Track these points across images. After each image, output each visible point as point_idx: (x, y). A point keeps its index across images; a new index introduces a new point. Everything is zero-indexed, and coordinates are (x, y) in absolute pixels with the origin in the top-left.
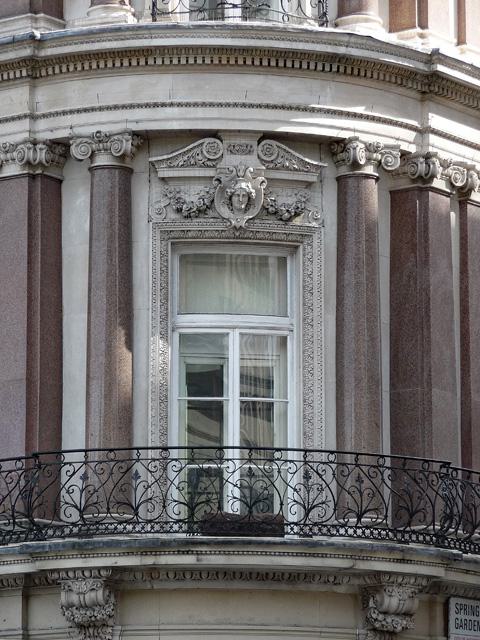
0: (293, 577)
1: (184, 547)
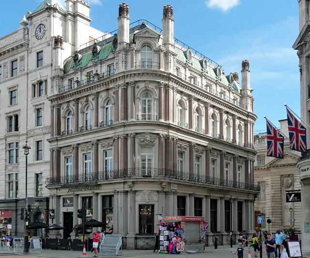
0: (153, 182)
1: (140, 179)
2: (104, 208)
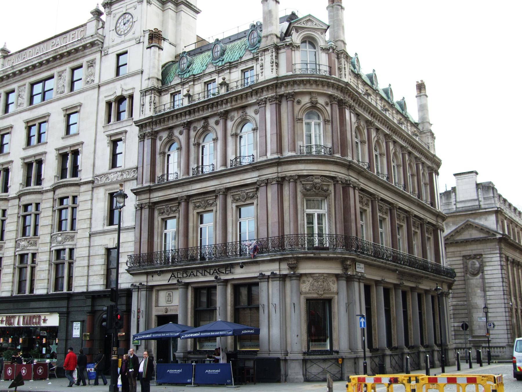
2: (237, 307)
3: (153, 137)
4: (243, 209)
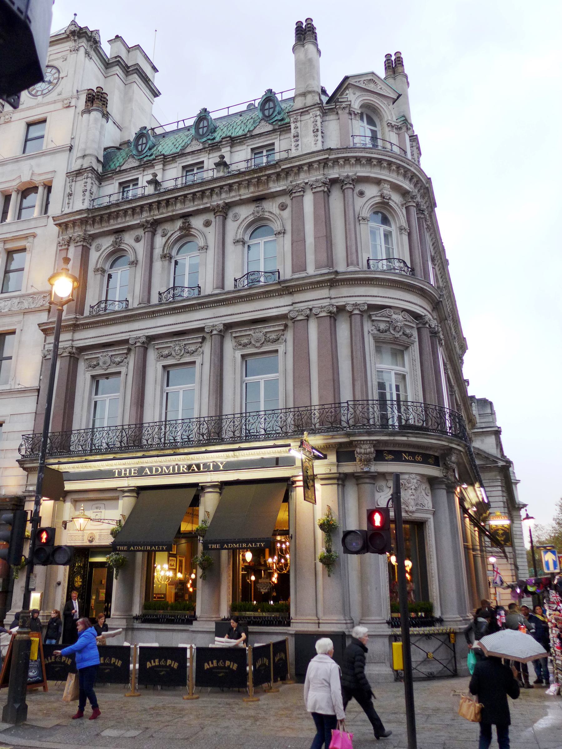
3: (84, 244)
4: (173, 372)
